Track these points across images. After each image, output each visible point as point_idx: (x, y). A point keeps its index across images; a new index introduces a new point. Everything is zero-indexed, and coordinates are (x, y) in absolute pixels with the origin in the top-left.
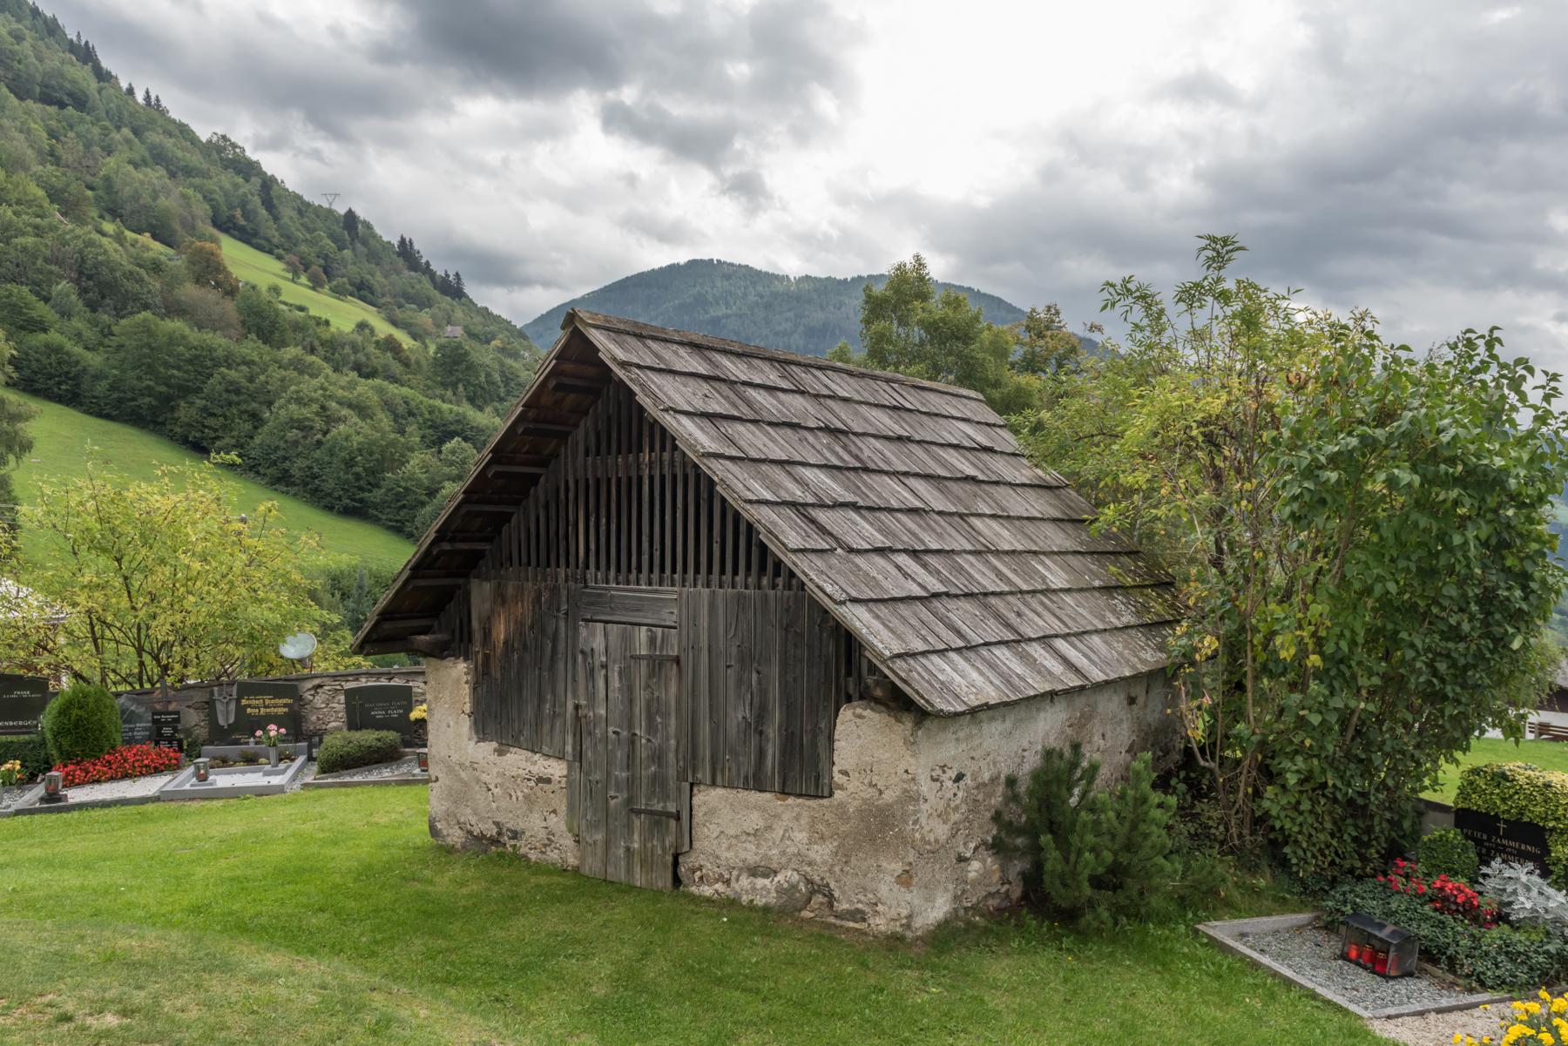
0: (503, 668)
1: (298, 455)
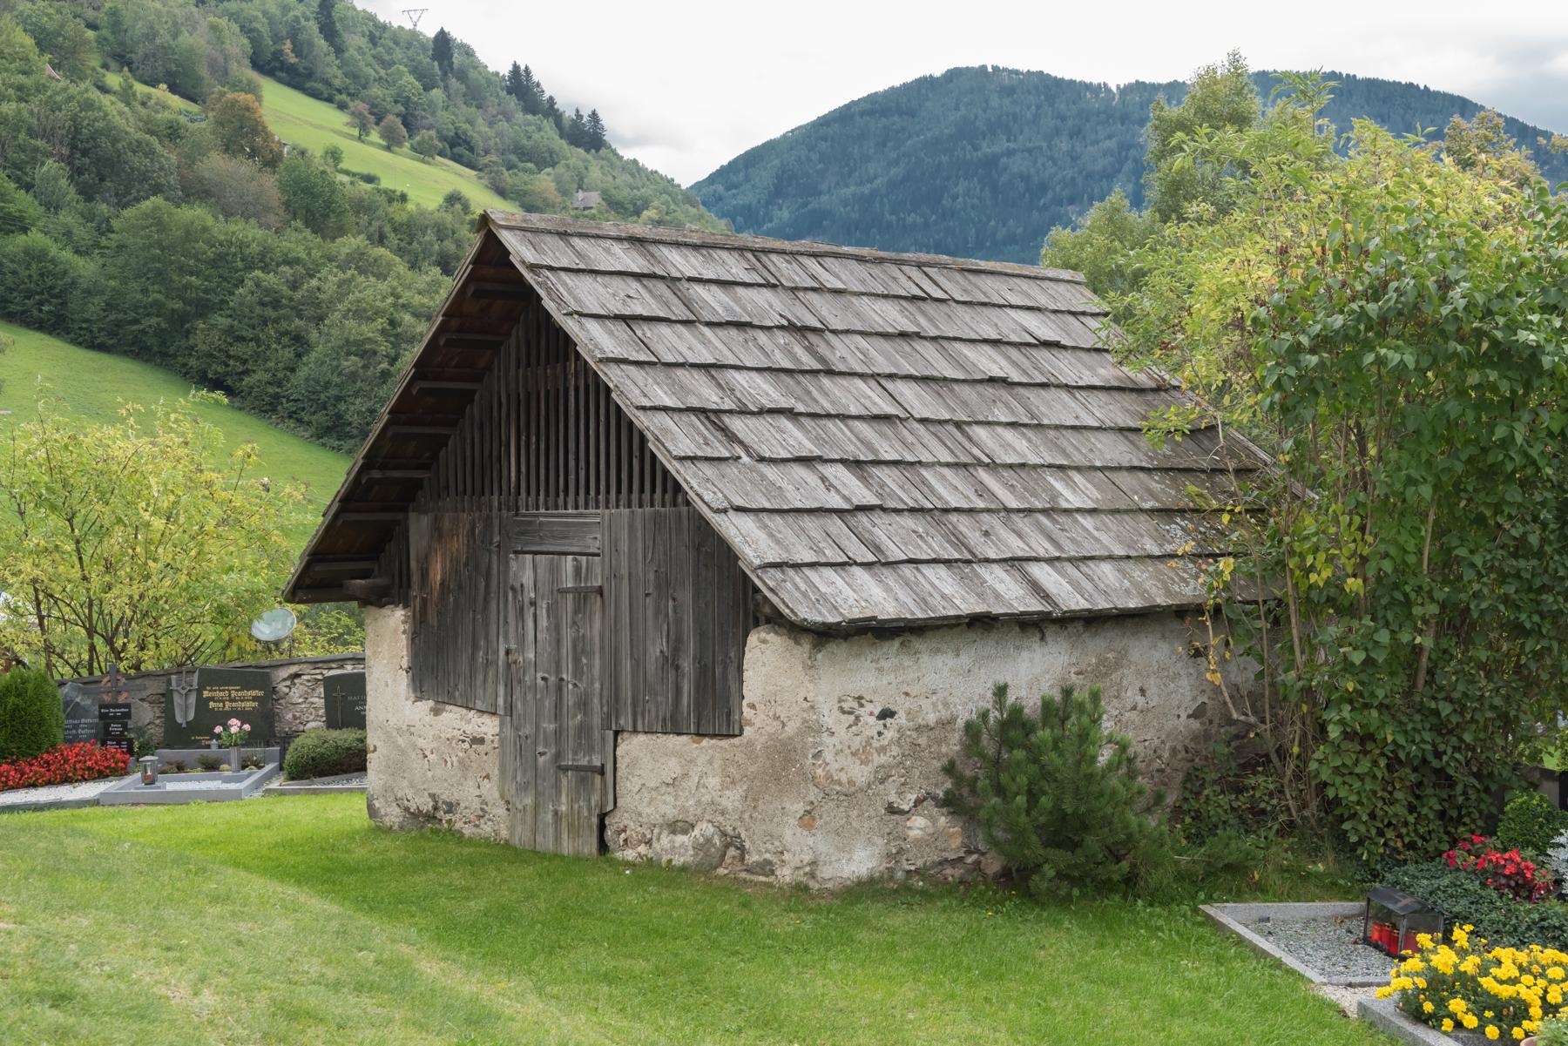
0: (439, 613)
1: (356, 395)
